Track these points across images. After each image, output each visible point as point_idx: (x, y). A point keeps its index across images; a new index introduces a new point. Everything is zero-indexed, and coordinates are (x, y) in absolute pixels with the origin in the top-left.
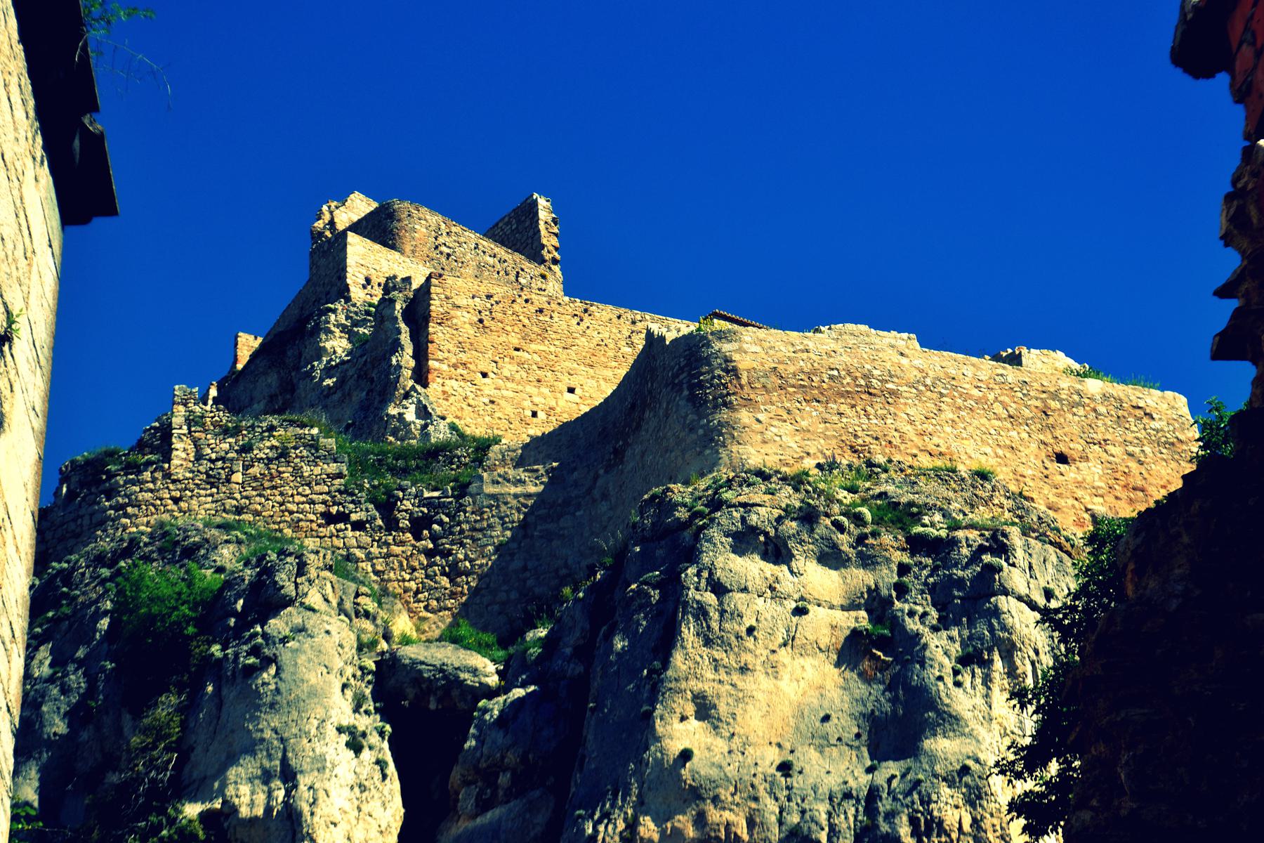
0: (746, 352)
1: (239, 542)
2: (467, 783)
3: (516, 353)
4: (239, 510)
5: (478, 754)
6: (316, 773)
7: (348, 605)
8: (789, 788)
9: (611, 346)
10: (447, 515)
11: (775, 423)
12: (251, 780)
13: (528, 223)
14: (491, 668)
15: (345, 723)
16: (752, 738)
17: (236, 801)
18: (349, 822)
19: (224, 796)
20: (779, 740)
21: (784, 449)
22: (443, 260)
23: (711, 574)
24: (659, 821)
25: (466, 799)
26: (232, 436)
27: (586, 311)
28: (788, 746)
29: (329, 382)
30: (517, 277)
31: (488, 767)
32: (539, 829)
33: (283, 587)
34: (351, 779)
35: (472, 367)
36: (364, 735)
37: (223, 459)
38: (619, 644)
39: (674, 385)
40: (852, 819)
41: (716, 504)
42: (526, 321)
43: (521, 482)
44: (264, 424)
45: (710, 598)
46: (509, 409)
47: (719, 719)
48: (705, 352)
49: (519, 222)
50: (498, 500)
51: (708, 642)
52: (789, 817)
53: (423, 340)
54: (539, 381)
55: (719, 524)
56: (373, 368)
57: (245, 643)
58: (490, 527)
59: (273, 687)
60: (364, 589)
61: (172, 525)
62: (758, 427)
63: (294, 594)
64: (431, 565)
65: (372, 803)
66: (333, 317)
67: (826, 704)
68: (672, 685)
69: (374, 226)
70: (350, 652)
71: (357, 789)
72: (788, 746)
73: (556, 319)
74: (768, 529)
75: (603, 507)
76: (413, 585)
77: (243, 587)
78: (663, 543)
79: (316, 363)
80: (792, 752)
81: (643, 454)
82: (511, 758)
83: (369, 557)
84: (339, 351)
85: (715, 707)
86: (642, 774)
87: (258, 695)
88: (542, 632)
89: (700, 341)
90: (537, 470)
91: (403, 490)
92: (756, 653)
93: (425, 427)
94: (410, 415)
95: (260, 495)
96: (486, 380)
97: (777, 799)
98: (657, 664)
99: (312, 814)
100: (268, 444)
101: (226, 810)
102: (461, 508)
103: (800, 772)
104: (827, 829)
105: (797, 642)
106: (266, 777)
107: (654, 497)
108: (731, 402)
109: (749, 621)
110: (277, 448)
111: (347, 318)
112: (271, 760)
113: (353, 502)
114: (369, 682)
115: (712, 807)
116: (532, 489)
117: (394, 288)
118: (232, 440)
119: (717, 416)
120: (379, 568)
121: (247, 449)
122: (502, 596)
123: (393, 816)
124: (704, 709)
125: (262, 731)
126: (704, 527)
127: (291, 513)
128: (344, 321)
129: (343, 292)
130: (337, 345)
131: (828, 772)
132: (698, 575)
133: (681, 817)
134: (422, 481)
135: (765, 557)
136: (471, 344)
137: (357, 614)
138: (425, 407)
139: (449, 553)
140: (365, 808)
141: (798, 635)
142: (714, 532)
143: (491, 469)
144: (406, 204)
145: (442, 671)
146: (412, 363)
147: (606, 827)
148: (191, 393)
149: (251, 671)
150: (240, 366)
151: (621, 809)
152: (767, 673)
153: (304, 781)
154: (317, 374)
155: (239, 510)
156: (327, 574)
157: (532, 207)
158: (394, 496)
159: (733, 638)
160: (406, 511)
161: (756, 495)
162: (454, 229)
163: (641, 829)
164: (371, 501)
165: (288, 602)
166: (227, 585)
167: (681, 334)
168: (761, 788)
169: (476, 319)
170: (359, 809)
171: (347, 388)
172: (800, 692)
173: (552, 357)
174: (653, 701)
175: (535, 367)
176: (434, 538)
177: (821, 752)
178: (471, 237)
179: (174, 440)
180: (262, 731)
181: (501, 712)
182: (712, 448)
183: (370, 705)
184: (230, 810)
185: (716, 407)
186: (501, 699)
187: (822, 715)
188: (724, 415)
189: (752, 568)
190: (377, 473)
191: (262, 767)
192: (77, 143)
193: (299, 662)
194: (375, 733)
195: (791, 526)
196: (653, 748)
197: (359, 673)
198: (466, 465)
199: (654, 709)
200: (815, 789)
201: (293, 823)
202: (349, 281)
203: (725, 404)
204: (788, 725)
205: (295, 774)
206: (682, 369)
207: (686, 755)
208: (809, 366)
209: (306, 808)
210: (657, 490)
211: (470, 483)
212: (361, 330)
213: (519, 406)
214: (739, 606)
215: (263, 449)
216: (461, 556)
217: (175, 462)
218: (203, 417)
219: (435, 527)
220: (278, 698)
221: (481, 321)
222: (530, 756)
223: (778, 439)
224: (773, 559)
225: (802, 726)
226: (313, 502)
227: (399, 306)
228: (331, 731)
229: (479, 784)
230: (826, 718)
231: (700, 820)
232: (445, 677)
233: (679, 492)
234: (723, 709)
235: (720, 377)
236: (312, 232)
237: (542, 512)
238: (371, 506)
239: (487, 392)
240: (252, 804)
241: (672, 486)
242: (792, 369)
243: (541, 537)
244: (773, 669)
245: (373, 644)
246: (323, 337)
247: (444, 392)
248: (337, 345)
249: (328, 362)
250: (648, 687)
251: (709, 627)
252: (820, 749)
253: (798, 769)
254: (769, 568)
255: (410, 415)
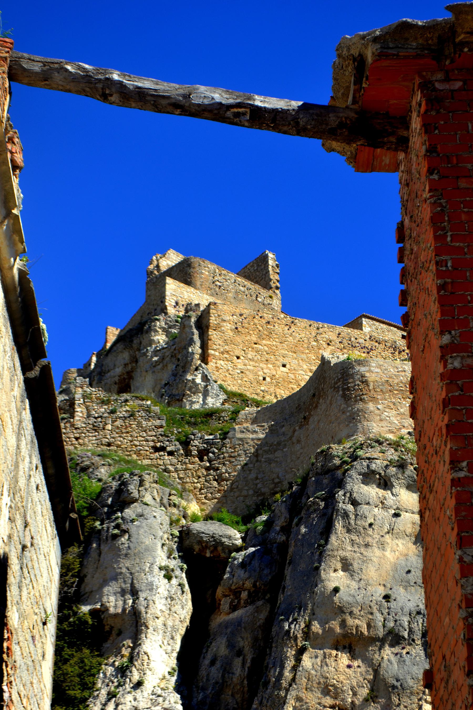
0: (372, 372)
1: (110, 465)
2: (225, 596)
3: (256, 345)
4: (109, 445)
5: (231, 582)
6: (148, 592)
7: (165, 501)
8: (389, 608)
9: (306, 341)
10: (217, 449)
11: (387, 410)
12: (115, 594)
13: (263, 267)
14: (238, 535)
15: (163, 564)
16: (370, 581)
17: (108, 604)
18: (165, 617)
19: (101, 601)
20: (384, 583)
21: (391, 424)
22: (217, 289)
23: (351, 495)
24: (322, 624)
25: (225, 604)
26: (106, 405)
27: (292, 322)
28: (389, 586)
29: (155, 359)
30: (257, 297)
31: (236, 589)
32: (261, 621)
33: (132, 493)
34: (166, 594)
35: (231, 353)
36: (173, 570)
37: (101, 417)
38: (303, 530)
39: (335, 388)
40: (420, 625)
41: (354, 458)
42: (261, 328)
43: (255, 432)
44: (122, 399)
45: (350, 508)
46: (251, 376)
47: (354, 571)
48: (351, 371)
49: (258, 266)
50: (243, 441)
51: (349, 531)
52: (388, 623)
53: (205, 338)
54: (267, 361)
55: (356, 468)
56: (179, 352)
57: (112, 522)
58: (239, 455)
59: (126, 545)
60: (173, 492)
61: (75, 454)
62: (377, 412)
63: (137, 496)
64: (208, 475)
65: (176, 607)
66: (158, 323)
67: (409, 564)
68: (330, 553)
69: (180, 271)
70: (166, 527)
71: (169, 599)
72: (389, 586)
73: (277, 327)
74: (381, 472)
75: (298, 447)
76: (199, 485)
77: (112, 491)
78: (327, 476)
79: (149, 348)
80: (391, 589)
81: (319, 422)
82: (248, 584)
83: (176, 470)
84: (161, 342)
85: (351, 565)
86: (314, 599)
87: (119, 550)
88: (264, 517)
89: (349, 365)
90: (264, 426)
91: (194, 435)
92: (374, 536)
93: (206, 386)
94: (198, 380)
95: (120, 437)
96: (239, 361)
97: (382, 614)
98: (322, 542)
99: (146, 613)
100: (124, 409)
101: (103, 609)
102: (224, 445)
103: (395, 600)
104: (408, 630)
105: (395, 531)
106: (123, 593)
107: (322, 451)
108: (364, 399)
109: (370, 520)
110: (129, 411)
111: (166, 324)
112: (125, 584)
113: (168, 441)
114: (175, 542)
115: (349, 617)
116: (262, 436)
117: (191, 310)
118: (106, 407)
119: (357, 406)
120: (181, 476)
121: (113, 412)
122: (245, 493)
123: (187, 612)
124: (346, 566)
125: (121, 568)
126: (347, 470)
127: (136, 446)
128: (164, 326)
129: (164, 310)
130: (160, 338)
131: (409, 600)
132: (344, 495)
133: (333, 622)
134: (204, 429)
135: (379, 486)
136: (231, 341)
137: (170, 505)
138: (206, 376)
139: (218, 469)
140: (173, 609)
141: (395, 528)
142: (353, 473)
143: (241, 423)
144: (198, 259)
145: (213, 537)
146: (200, 351)
147: (295, 626)
148: (85, 381)
149: (115, 537)
150: (109, 345)
151: (303, 616)
152: (379, 547)
153: (142, 595)
154: (149, 354)
155: (109, 445)
156: (155, 485)
157: (265, 259)
158: (189, 438)
159: (362, 529)
160: (195, 446)
161: (374, 453)
162: (223, 272)
163: (313, 627)
164: (178, 440)
165: (134, 501)
166: (103, 490)
167: (339, 360)
168: (375, 608)
169: (234, 327)
170: (170, 610)
171: (165, 362)
172: (396, 557)
173: (275, 348)
174: (320, 562)
175: (265, 353)
176: (210, 461)
177: (406, 589)
178: (233, 276)
179: (76, 407)
180: (121, 568)
181: (243, 560)
182: (354, 423)
183: (176, 554)
184: (104, 609)
185: (356, 401)
186: (243, 553)
187: (407, 570)
188: (360, 405)
189: (372, 492)
190: (180, 425)
191: (121, 587)
192: (68, 523)
193: (140, 532)
194: (179, 569)
195: (393, 470)
196: (319, 586)
197: (171, 537)
198: (227, 421)
199: (321, 565)
200: (402, 609)
201: (136, 617)
202: (167, 304)
203: (361, 400)
204: (389, 575)
205: (138, 591)
206: (339, 380)
207: (336, 590)
208: (405, 379)
209: (143, 610)
210: (325, 447)
211: (228, 432)
212: (173, 331)
213: (256, 374)
214: (365, 512)
215: (122, 412)
216: (224, 471)
217: (77, 418)
218: (91, 394)
219: (211, 455)
220: (129, 551)
221: (236, 328)
222: (258, 584)
223: (388, 418)
224: (383, 487)
225: (396, 576)
226: (147, 441)
227: (193, 320)
228: (156, 569)
229: (232, 597)
230: (409, 572)
231: (343, 624)
232: (215, 541)
233: (337, 449)
234: (356, 566)
235: (358, 385)
236: (147, 272)
237: (266, 448)
238: (177, 443)
239: (239, 367)
240: (116, 607)
241: (332, 445)
242: (396, 381)
243: (266, 462)
244: (382, 545)
245: (178, 520)
246: (153, 334)
247: (217, 367)
248: (160, 338)
249: (155, 348)
250: (318, 553)
251: (349, 523)
252: (406, 588)
253: (394, 598)
254: (381, 492)
255: (198, 380)
